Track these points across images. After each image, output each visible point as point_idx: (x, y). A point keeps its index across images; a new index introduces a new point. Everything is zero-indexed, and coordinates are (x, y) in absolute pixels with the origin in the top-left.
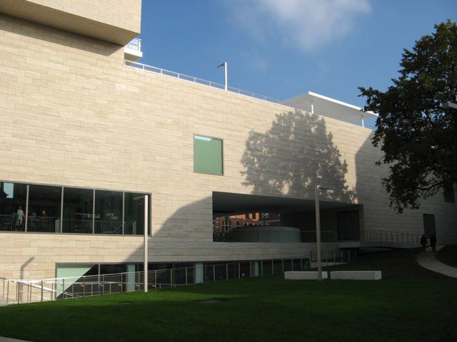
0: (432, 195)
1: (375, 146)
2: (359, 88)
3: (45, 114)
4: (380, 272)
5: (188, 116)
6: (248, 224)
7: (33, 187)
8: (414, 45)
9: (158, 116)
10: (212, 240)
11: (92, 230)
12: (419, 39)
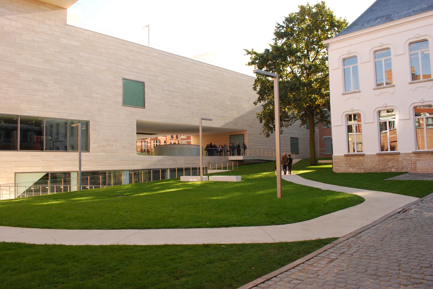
0: (291, 125)
1: (255, 90)
2: (244, 50)
4: (319, 161)
8: (284, 19)
11: (17, 146)
12: (288, 16)
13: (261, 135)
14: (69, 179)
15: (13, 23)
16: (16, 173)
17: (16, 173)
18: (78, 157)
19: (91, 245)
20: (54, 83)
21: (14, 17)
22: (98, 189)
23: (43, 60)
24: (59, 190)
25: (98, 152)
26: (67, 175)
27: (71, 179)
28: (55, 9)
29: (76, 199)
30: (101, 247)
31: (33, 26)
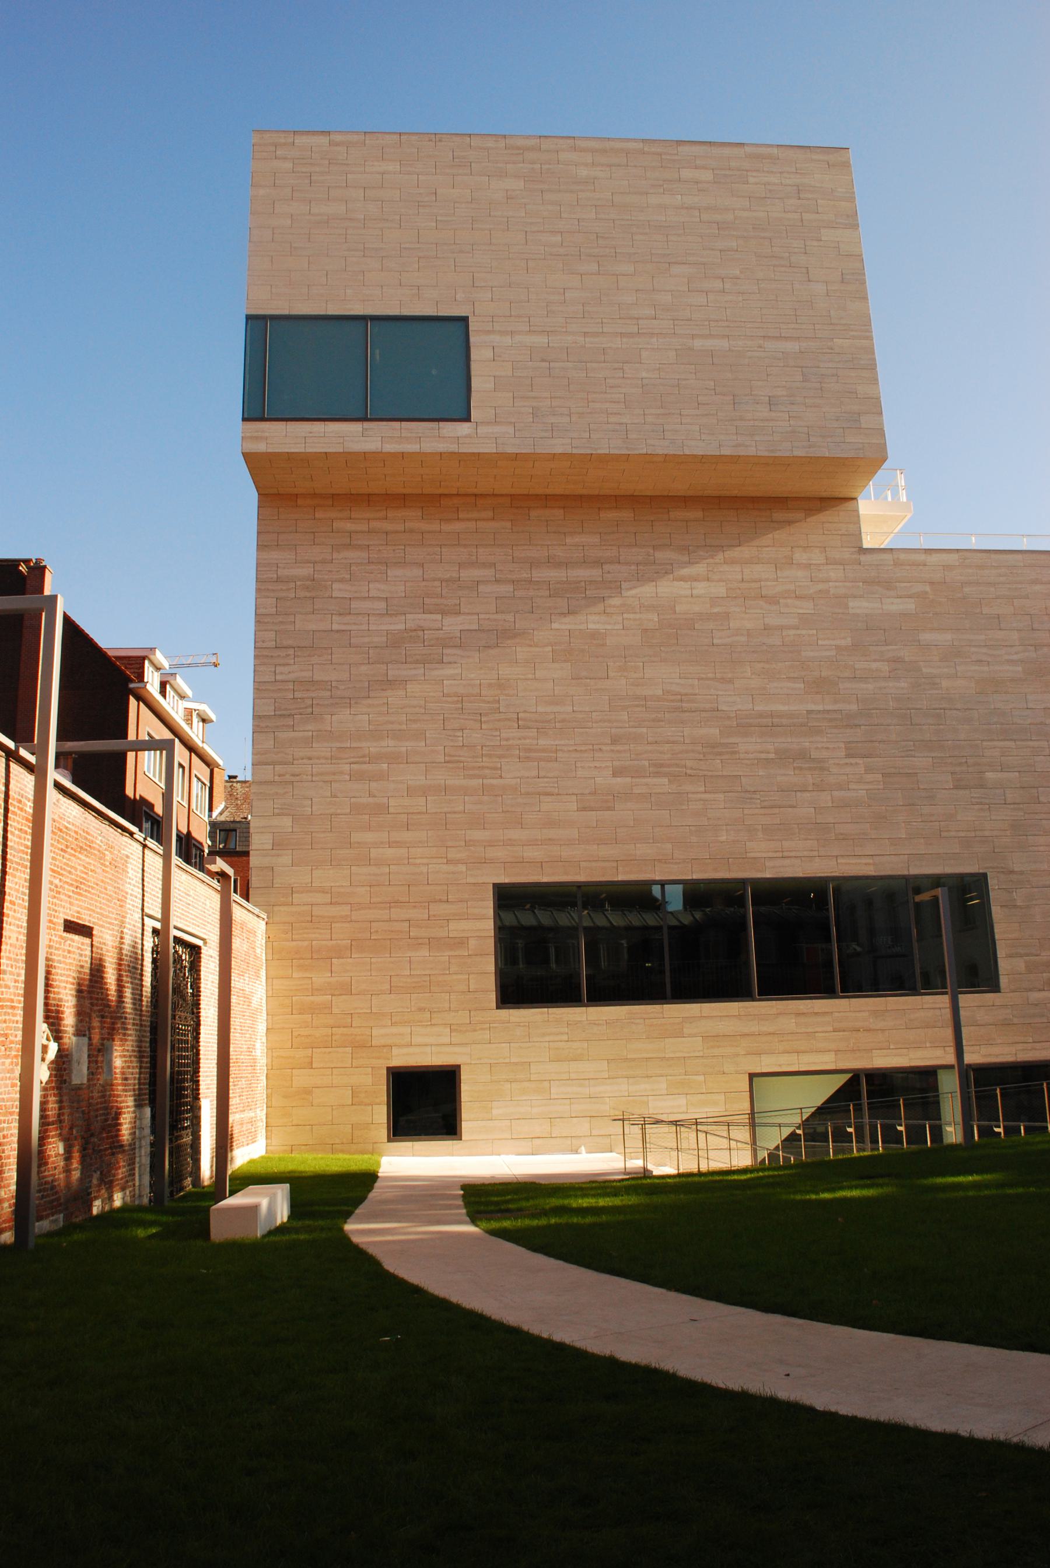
13: (54, 804)
14: (934, 1096)
15: (701, 588)
16: (752, 1076)
17: (752, 1076)
18: (947, 1013)
19: (911, 1423)
20: (848, 756)
21: (700, 569)
22: (1038, 1139)
23: (802, 686)
24: (891, 1136)
25: (1030, 990)
26: (927, 1076)
27: (941, 1096)
28: (820, 510)
29: (940, 1180)
30: (951, 1440)
31: (760, 581)
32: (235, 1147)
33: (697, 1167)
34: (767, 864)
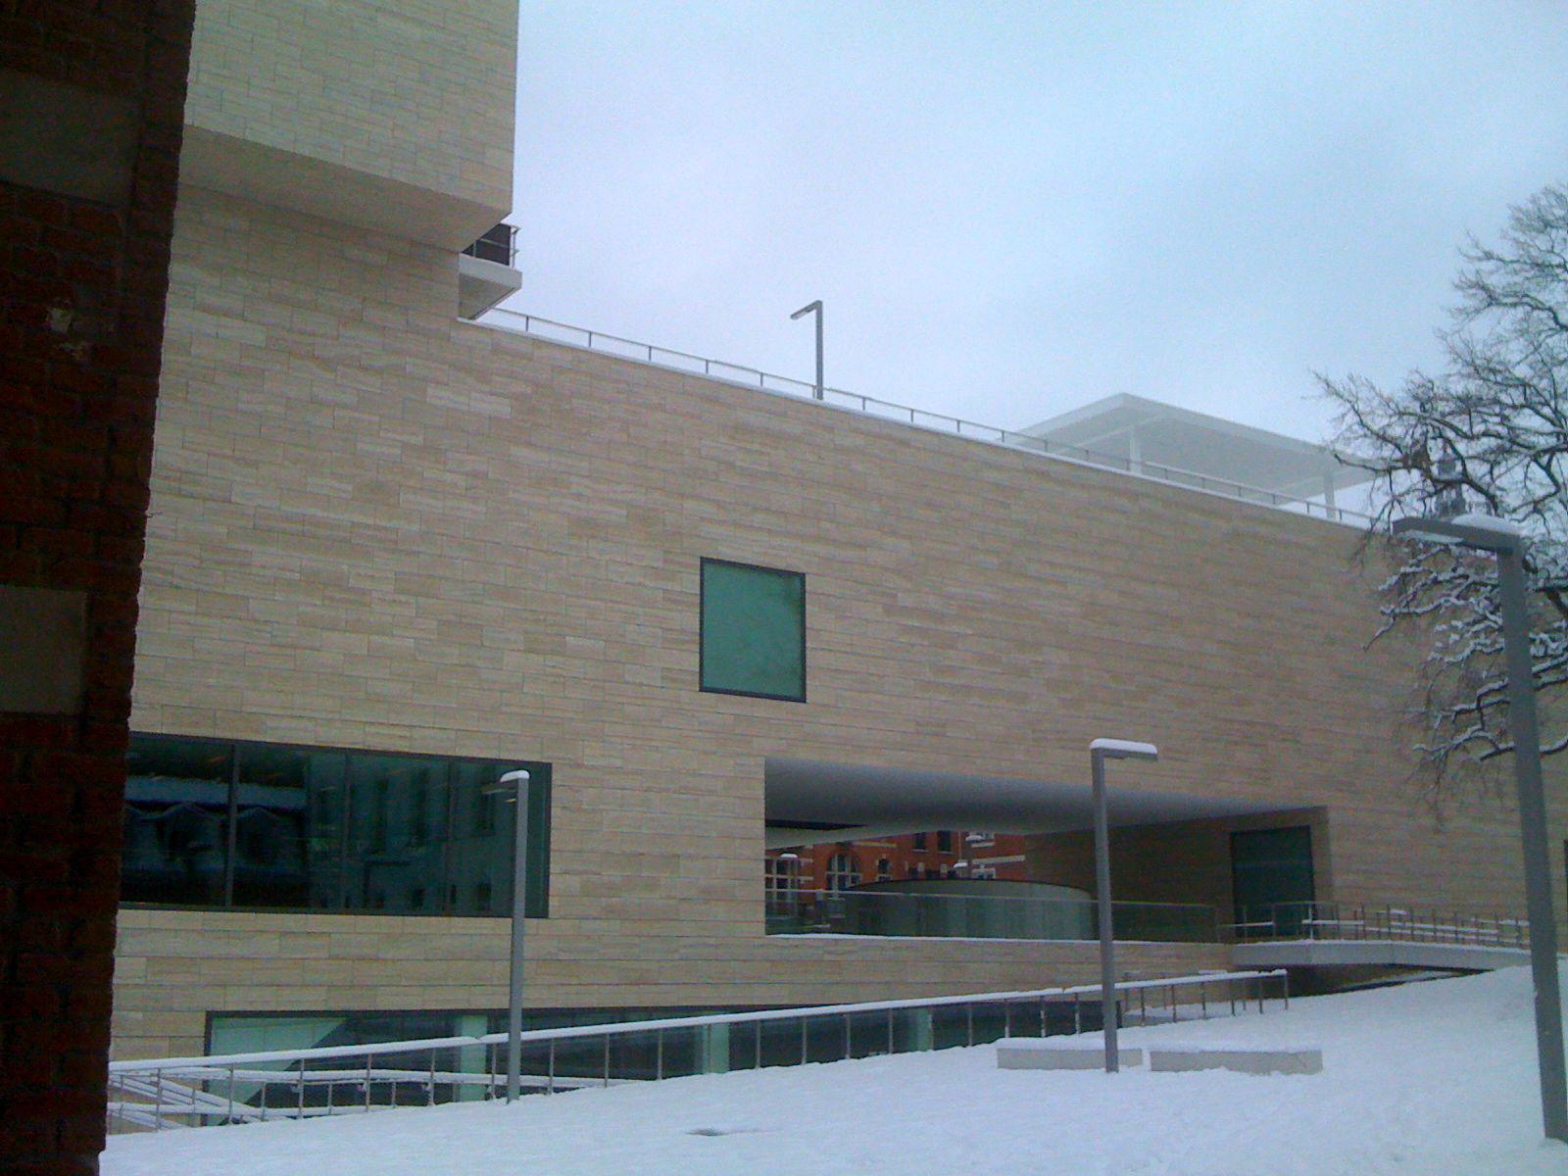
3: (179, 493)
5: (682, 496)
6: (921, 867)
7: (887, 1051)
9: (579, 496)
10: (556, 777)
32: (727, 1041)
33: (1235, 1007)
34: (269, 724)
